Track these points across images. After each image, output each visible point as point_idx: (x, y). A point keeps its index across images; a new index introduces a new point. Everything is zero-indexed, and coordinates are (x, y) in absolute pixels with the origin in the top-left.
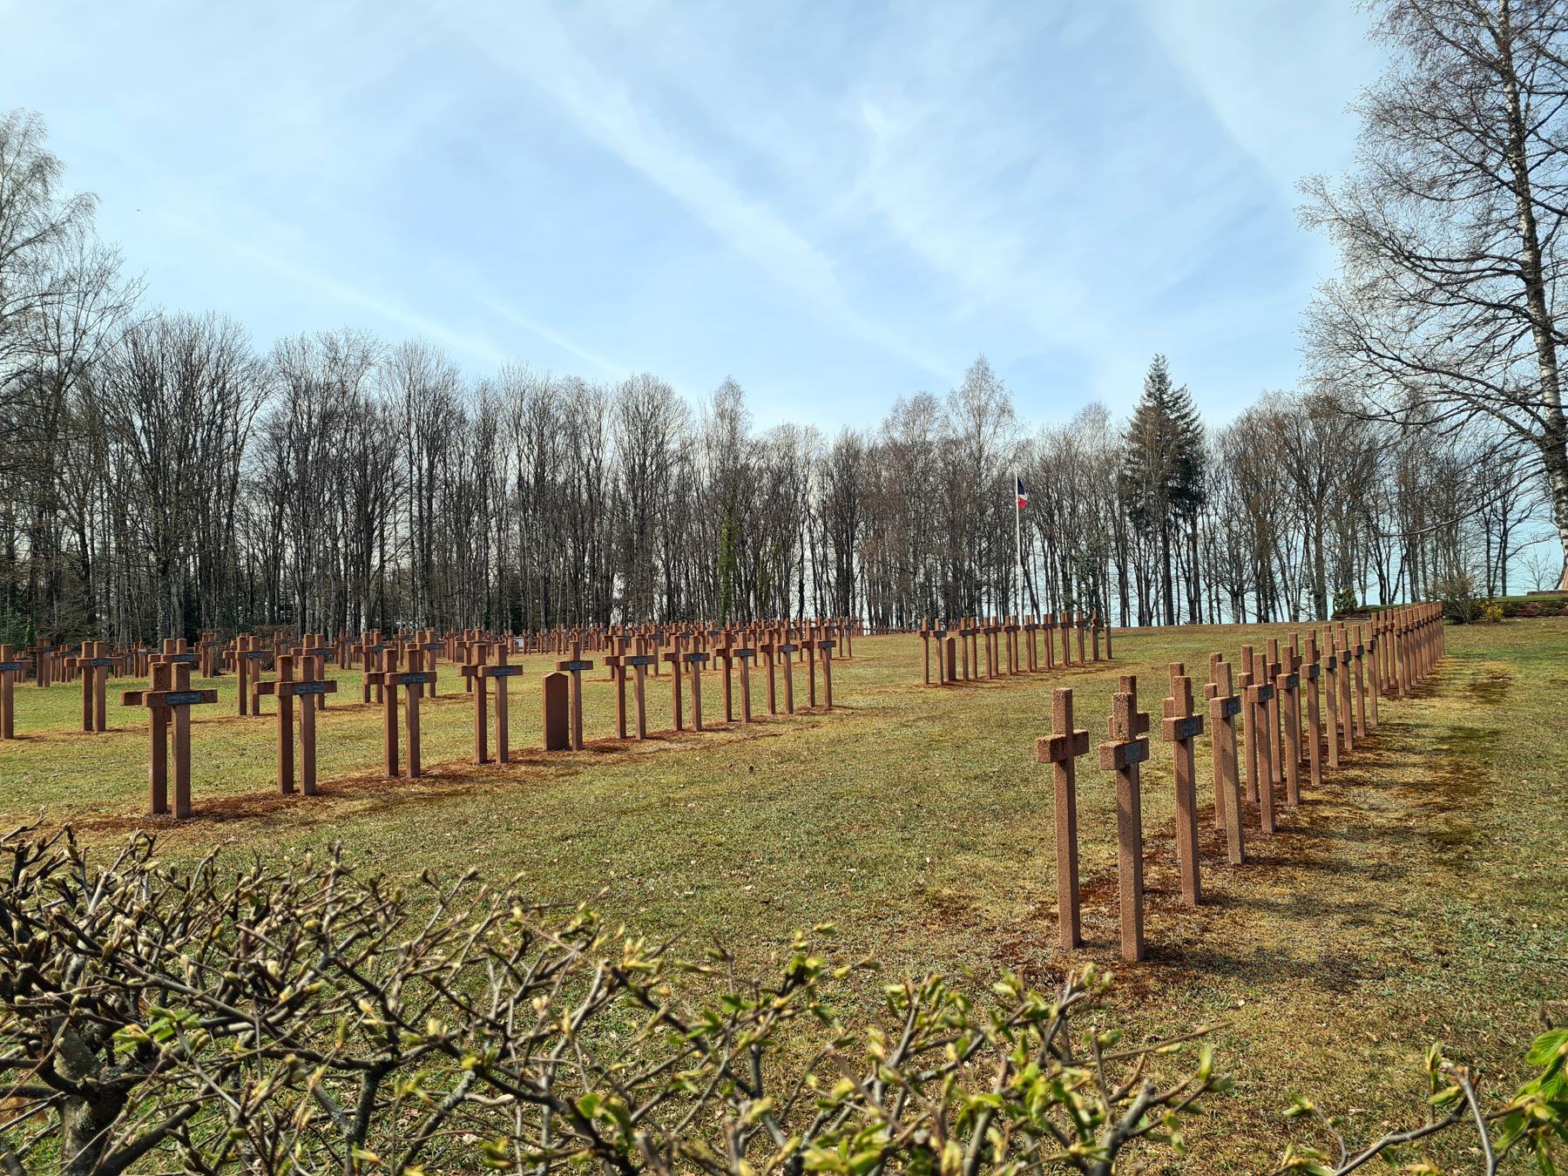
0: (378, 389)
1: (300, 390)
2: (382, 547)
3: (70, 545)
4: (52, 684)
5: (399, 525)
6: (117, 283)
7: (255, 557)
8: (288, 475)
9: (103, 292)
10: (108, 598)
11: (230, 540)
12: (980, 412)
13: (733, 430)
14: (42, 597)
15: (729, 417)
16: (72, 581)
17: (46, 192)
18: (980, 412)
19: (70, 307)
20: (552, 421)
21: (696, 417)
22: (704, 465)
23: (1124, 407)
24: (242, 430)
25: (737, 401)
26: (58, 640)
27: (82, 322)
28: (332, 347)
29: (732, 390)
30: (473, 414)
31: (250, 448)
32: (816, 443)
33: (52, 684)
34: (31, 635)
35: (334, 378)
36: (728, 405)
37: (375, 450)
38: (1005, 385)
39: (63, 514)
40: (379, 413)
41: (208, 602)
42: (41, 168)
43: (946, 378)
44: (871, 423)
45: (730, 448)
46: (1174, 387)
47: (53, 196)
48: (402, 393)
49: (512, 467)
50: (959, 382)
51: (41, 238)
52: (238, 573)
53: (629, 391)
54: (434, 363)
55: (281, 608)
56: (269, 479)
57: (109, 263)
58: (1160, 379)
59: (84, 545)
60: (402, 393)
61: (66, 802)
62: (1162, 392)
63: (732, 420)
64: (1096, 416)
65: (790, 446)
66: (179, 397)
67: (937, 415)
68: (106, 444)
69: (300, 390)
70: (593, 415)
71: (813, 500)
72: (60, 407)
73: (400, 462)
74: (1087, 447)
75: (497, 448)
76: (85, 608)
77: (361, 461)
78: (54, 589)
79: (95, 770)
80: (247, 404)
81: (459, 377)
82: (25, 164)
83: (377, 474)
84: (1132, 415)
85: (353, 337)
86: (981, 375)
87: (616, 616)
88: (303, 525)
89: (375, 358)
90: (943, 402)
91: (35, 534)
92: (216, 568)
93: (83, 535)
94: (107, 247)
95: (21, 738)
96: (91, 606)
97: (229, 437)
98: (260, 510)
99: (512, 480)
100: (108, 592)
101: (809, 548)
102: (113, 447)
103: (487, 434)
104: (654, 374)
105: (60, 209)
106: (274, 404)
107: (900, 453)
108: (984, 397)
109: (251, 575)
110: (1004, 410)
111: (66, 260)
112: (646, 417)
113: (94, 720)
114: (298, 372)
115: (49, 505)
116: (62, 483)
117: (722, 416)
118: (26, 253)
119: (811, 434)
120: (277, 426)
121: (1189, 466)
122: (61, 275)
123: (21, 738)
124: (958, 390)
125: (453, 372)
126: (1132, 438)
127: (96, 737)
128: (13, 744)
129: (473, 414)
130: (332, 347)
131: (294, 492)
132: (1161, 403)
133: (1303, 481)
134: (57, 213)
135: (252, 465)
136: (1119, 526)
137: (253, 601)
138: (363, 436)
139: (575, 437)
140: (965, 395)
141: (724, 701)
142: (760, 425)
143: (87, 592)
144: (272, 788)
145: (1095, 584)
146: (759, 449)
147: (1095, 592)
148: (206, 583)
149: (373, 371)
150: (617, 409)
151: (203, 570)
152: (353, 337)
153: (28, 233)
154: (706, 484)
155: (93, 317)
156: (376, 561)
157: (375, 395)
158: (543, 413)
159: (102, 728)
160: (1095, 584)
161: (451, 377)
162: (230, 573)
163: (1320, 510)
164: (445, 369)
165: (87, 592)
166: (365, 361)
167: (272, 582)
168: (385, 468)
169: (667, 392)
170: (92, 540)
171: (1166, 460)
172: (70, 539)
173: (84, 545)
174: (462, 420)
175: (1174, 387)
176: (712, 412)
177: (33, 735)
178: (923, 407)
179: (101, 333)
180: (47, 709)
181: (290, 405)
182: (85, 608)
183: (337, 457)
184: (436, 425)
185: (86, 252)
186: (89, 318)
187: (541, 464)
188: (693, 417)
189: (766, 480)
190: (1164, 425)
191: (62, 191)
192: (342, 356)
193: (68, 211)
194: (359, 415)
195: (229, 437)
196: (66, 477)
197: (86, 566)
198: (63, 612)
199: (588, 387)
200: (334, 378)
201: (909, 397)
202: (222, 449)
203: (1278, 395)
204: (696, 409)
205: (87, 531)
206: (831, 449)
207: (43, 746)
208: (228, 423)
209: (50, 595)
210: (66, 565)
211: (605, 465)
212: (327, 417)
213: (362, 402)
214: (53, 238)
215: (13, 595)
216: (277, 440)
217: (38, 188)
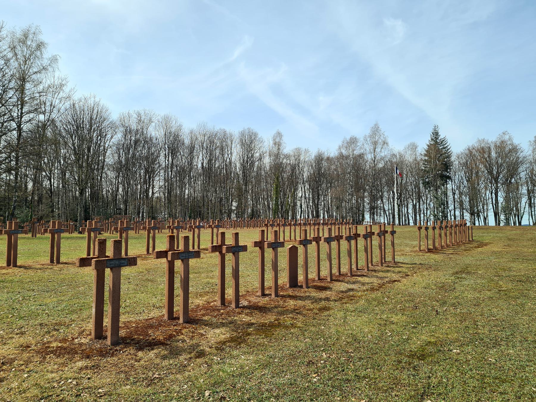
0: (155, 132)
1: (128, 132)
2: (153, 188)
3: (46, 185)
4: (38, 235)
5: (159, 182)
6: (67, 89)
7: (109, 191)
8: (122, 162)
9: (61, 93)
10: (58, 204)
11: (101, 185)
12: (375, 143)
13: (279, 149)
14: (36, 203)
15: (278, 144)
16: (46, 198)
17: (41, 54)
18: (375, 143)
19: (50, 97)
20: (216, 144)
21: (266, 144)
22: (267, 161)
23: (423, 143)
24: (106, 146)
25: (281, 139)
26: (40, 219)
27: (54, 103)
28: (139, 115)
29: (279, 135)
30: (187, 142)
31: (109, 152)
32: (308, 155)
33: (38, 235)
34: (31, 216)
35: (139, 127)
36: (277, 140)
37: (152, 154)
38: (385, 133)
39: (44, 173)
40: (154, 141)
41: (93, 206)
42: (40, 46)
43: (360, 131)
44: (331, 148)
45: (277, 156)
46: (441, 137)
47: (44, 56)
48: (163, 133)
49: (200, 161)
50: (368, 132)
51: (39, 72)
52: (103, 196)
53: (242, 134)
54: (174, 122)
55: (117, 209)
56: (115, 164)
57: (63, 83)
58: (436, 134)
59: (51, 186)
60: (163, 133)
61: (39, 321)
62: (437, 139)
63: (279, 145)
64: (413, 147)
65: (299, 156)
66: (86, 131)
67: (359, 144)
68: (60, 149)
69: (128, 132)
70: (229, 143)
71: (305, 175)
72: (44, 135)
73: (162, 158)
74: (409, 158)
75: (195, 154)
76: (51, 207)
77: (147, 158)
78: (40, 201)
79: (55, 291)
80: (109, 136)
81: (183, 127)
82: (34, 45)
83: (153, 162)
84: (426, 147)
85: (147, 112)
86: (376, 130)
87: (233, 216)
88: (126, 178)
89: (153, 119)
90: (362, 139)
91: (35, 181)
92: (95, 196)
93: (51, 181)
94: (63, 76)
95: (20, 267)
96: (52, 207)
97: (102, 148)
98: (111, 174)
99: (200, 165)
100: (58, 202)
101: (302, 192)
102: (62, 151)
103: (192, 149)
104: (252, 128)
105: (46, 61)
106: (119, 137)
107: (341, 157)
108: (377, 138)
109: (107, 197)
110: (385, 143)
111: (48, 81)
112: (248, 143)
113: (55, 258)
114: (127, 125)
115: (39, 169)
116: (44, 163)
117: (275, 144)
118: (34, 76)
119: (307, 151)
120: (118, 144)
121: (447, 166)
122: (47, 86)
123: (20, 267)
124: (367, 134)
125: (180, 126)
126: (425, 155)
127: (56, 268)
128: (16, 270)
129: (187, 142)
130: (139, 115)
131: (124, 168)
132: (436, 142)
133: (490, 173)
134: (45, 62)
135: (110, 159)
136: (417, 186)
137: (107, 206)
138: (149, 149)
139: (222, 149)
140: (370, 136)
141: (316, 254)
142: (288, 149)
143: (51, 202)
144: (155, 313)
145: (444, 208)
146: (287, 157)
147: (444, 211)
148: (92, 199)
149: (153, 124)
150: (238, 140)
151: (92, 195)
152: (147, 112)
153: (35, 70)
154: (268, 168)
155: (58, 101)
156: (150, 194)
157: (153, 134)
158: (212, 142)
159: (58, 262)
160: (444, 208)
161: (180, 127)
162: (100, 196)
163: (497, 182)
164: (178, 124)
165: (51, 202)
166: (151, 121)
167: (115, 199)
168: (155, 160)
169: (256, 135)
170: (54, 183)
171: (438, 164)
172: (46, 183)
173: (51, 186)
174: (183, 144)
175: (441, 137)
176: (271, 143)
177: (26, 264)
178: (353, 141)
179: (60, 111)
180: (34, 248)
181: (124, 136)
182: (51, 207)
183: (138, 154)
184: (174, 145)
185: (56, 78)
186: (56, 102)
187: (210, 161)
188: (265, 143)
189: (288, 168)
190: (438, 151)
191: (47, 54)
192: (142, 119)
193: (49, 62)
194: (148, 141)
195: (102, 148)
196: (46, 160)
197: (51, 192)
198: (43, 209)
199: (228, 132)
200: (139, 127)
201: (348, 138)
202: (100, 152)
203: (483, 140)
204: (266, 140)
205: (52, 180)
206: (313, 157)
207: (31, 272)
208: (102, 144)
209: (38, 202)
210: (45, 192)
211: (233, 160)
212: (136, 142)
213: (149, 136)
214: (44, 71)
215: (26, 202)
216: (118, 149)
217: (38, 53)
